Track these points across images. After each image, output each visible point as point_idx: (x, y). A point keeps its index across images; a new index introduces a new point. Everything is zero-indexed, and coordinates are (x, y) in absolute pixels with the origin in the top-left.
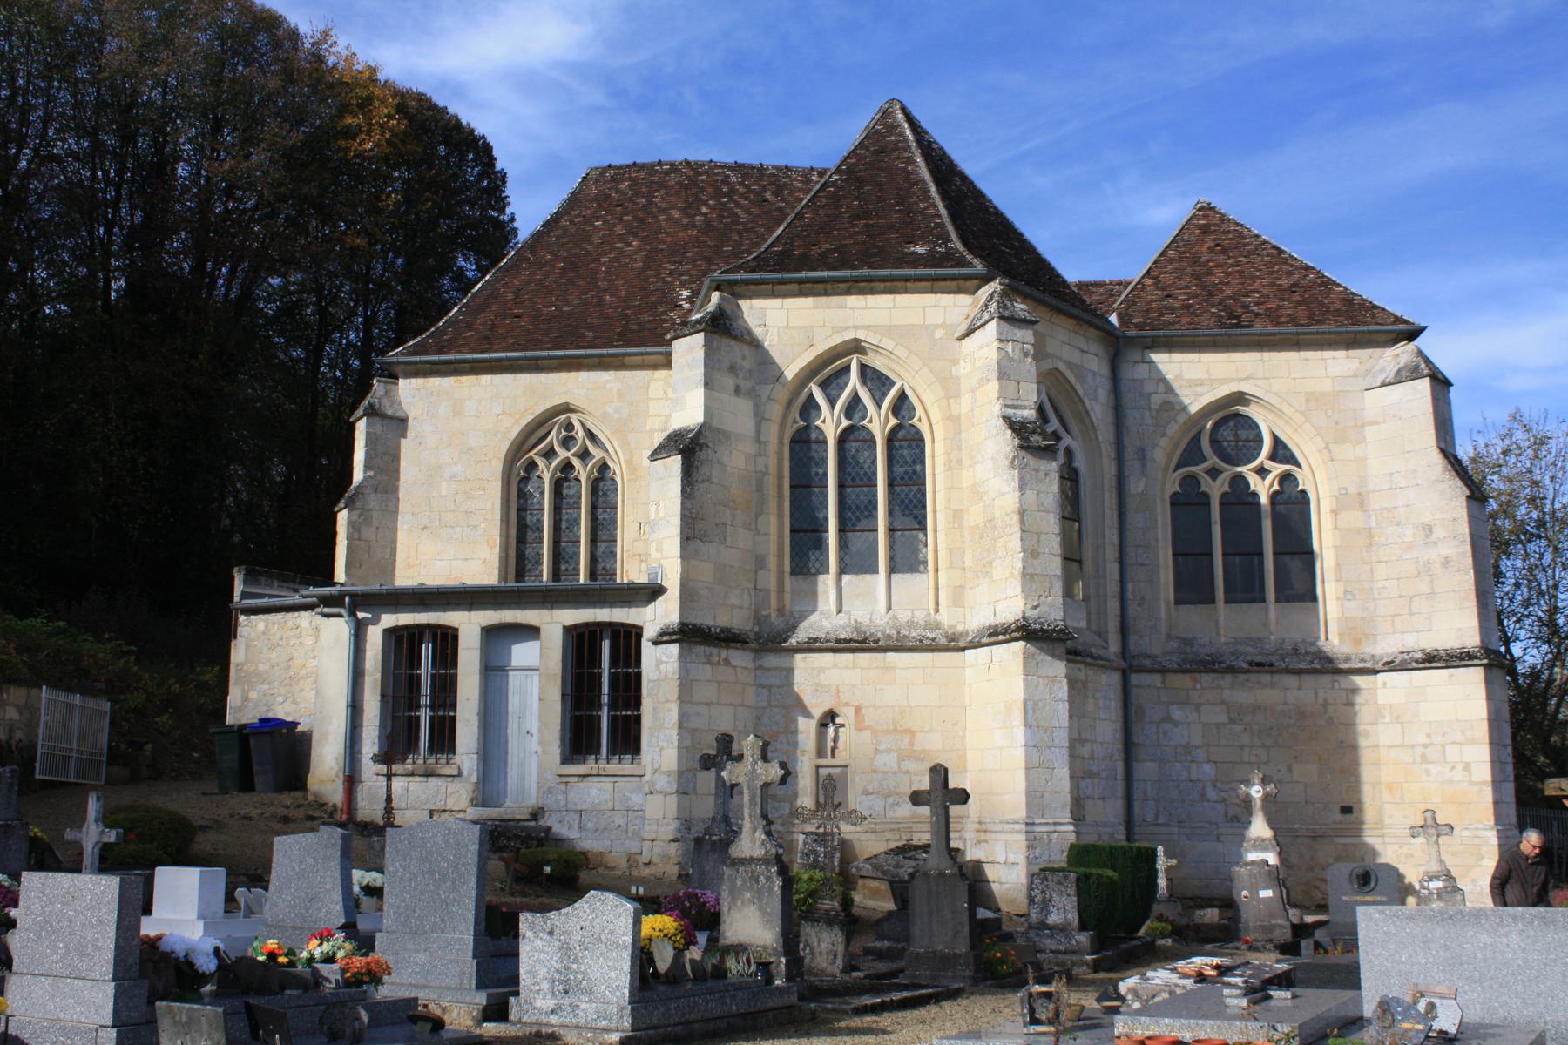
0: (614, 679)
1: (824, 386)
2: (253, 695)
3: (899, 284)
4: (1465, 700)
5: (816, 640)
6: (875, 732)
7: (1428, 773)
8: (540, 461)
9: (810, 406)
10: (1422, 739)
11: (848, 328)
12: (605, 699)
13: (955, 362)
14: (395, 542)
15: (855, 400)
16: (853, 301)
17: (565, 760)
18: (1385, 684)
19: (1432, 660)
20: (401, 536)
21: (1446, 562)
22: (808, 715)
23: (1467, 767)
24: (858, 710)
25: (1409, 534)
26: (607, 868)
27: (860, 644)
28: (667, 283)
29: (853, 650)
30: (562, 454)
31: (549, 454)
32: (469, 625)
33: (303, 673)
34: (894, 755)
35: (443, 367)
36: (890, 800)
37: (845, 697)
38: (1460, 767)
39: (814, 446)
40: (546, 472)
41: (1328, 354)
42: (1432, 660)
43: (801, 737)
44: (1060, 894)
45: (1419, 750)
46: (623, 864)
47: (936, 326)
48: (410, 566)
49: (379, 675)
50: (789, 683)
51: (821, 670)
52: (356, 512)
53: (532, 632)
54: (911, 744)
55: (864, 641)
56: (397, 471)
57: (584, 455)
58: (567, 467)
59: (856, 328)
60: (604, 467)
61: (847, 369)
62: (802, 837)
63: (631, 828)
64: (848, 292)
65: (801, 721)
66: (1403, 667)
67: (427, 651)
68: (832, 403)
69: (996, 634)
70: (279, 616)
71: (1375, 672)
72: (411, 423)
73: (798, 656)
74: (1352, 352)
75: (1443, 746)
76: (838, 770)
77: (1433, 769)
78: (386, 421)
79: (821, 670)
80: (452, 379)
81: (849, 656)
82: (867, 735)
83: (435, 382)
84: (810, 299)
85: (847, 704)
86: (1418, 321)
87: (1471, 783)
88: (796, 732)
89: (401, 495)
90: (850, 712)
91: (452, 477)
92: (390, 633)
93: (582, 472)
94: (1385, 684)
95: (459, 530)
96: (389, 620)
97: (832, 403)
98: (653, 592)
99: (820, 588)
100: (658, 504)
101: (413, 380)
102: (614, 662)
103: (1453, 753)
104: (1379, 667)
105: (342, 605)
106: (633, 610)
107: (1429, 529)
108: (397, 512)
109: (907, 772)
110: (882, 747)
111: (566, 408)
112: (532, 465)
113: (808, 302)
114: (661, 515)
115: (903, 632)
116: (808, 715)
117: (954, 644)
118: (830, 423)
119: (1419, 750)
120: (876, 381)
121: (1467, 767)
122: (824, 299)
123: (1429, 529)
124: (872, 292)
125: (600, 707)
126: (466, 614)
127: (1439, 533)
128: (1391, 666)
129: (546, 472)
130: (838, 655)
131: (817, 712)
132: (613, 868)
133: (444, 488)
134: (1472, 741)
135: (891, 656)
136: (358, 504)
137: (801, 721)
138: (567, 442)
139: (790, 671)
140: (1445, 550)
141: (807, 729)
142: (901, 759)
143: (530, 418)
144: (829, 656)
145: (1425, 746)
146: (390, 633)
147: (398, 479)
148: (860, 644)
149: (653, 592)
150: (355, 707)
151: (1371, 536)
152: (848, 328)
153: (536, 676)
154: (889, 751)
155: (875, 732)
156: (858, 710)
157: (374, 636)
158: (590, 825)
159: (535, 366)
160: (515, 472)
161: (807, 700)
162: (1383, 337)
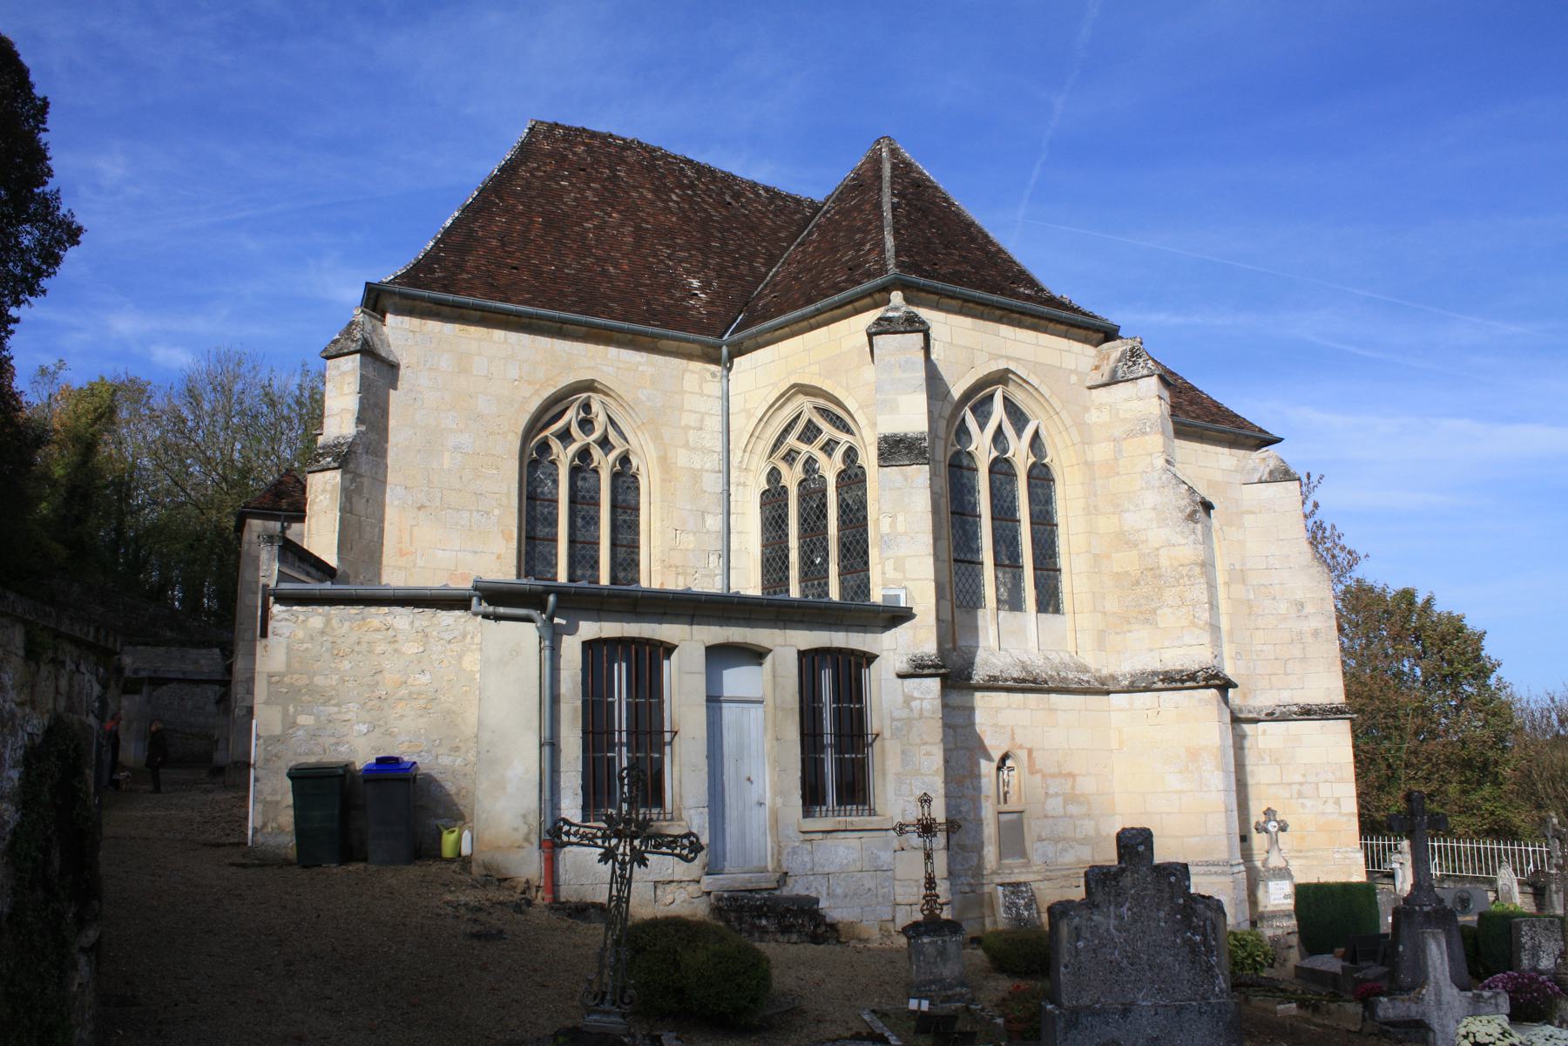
0: (838, 714)
1: (973, 410)
2: (304, 720)
3: (1043, 322)
4: (1332, 748)
5: (995, 678)
6: (1044, 776)
7: (1303, 806)
8: (556, 445)
9: (962, 432)
10: (1298, 778)
11: (1001, 356)
12: (828, 739)
13: (1086, 409)
14: (382, 520)
15: (999, 430)
16: (1005, 330)
17: (807, 814)
18: (1264, 732)
19: (1307, 713)
20: (391, 514)
21: (1316, 633)
22: (990, 759)
23: (1337, 801)
24: (1030, 751)
25: (1283, 607)
26: (860, 940)
27: (1030, 684)
28: (669, 267)
29: (1023, 690)
30: (580, 439)
31: (565, 436)
32: (689, 642)
33: (403, 692)
34: (1060, 799)
35: (447, 310)
36: (1060, 846)
37: (1019, 740)
38: (1331, 802)
39: (966, 473)
40: (564, 456)
41: (1219, 449)
42: (1307, 713)
43: (984, 781)
44: (1548, 940)
45: (1296, 788)
46: (875, 934)
47: (1071, 371)
48: (402, 554)
49: (579, 703)
50: (971, 723)
51: (998, 710)
52: (349, 476)
53: (756, 655)
54: (1073, 788)
55: (1034, 681)
56: (386, 429)
57: (604, 443)
58: (584, 454)
59: (1008, 358)
60: (625, 460)
61: (991, 396)
62: (1000, 889)
63: (881, 891)
64: (1000, 320)
65: (983, 763)
66: (1284, 718)
67: (620, 672)
68: (982, 427)
69: (1173, 680)
70: (353, 610)
71: (1257, 721)
72: (402, 372)
73: (978, 695)
74: (1234, 451)
75: (1317, 784)
76: (1014, 816)
77: (1308, 803)
78: (378, 364)
79: (998, 710)
80: (457, 327)
81: (1019, 696)
82: (1038, 777)
83: (433, 326)
84: (969, 321)
85: (1021, 747)
86: (1278, 435)
87: (1340, 814)
88: (979, 776)
89: (390, 461)
90: (1023, 754)
91: (457, 448)
92: (588, 646)
93: (604, 463)
94: (1264, 732)
95: (466, 514)
96: (590, 629)
97: (982, 427)
98: (896, 616)
99: (981, 623)
100: (894, 517)
101: (407, 319)
102: (837, 697)
103: (1325, 790)
104: (1263, 716)
105: (542, 607)
106: (869, 636)
107: (1300, 605)
108: (384, 482)
109: (1071, 817)
110: (1051, 791)
111: (590, 386)
112: (544, 447)
113: (967, 322)
114: (901, 527)
115: (1063, 674)
116: (990, 759)
117: (1101, 688)
118: (981, 447)
119: (1296, 788)
120: (1017, 417)
121: (1337, 801)
122: (980, 322)
123: (1300, 605)
124: (1020, 325)
125: (823, 748)
126: (687, 627)
127: (1309, 609)
128: (1272, 717)
129: (564, 456)
130: (1011, 695)
131: (997, 755)
132: (867, 941)
133: (447, 461)
134: (1341, 780)
135: (1053, 696)
136: (352, 466)
137: (983, 763)
138: (586, 424)
139: (971, 710)
140: (1314, 623)
141: (987, 768)
142: (1066, 803)
143: (553, 390)
144: (1003, 695)
145: (1301, 784)
146: (588, 646)
147: (386, 441)
148: (1030, 684)
149: (896, 616)
150: (551, 745)
151: (1251, 607)
152: (1001, 356)
153: (756, 712)
154: (1057, 795)
155: (1044, 776)
156: (1030, 751)
157: (571, 648)
158: (839, 891)
159: (559, 330)
160: (528, 452)
161: (988, 741)
162: (1252, 442)
